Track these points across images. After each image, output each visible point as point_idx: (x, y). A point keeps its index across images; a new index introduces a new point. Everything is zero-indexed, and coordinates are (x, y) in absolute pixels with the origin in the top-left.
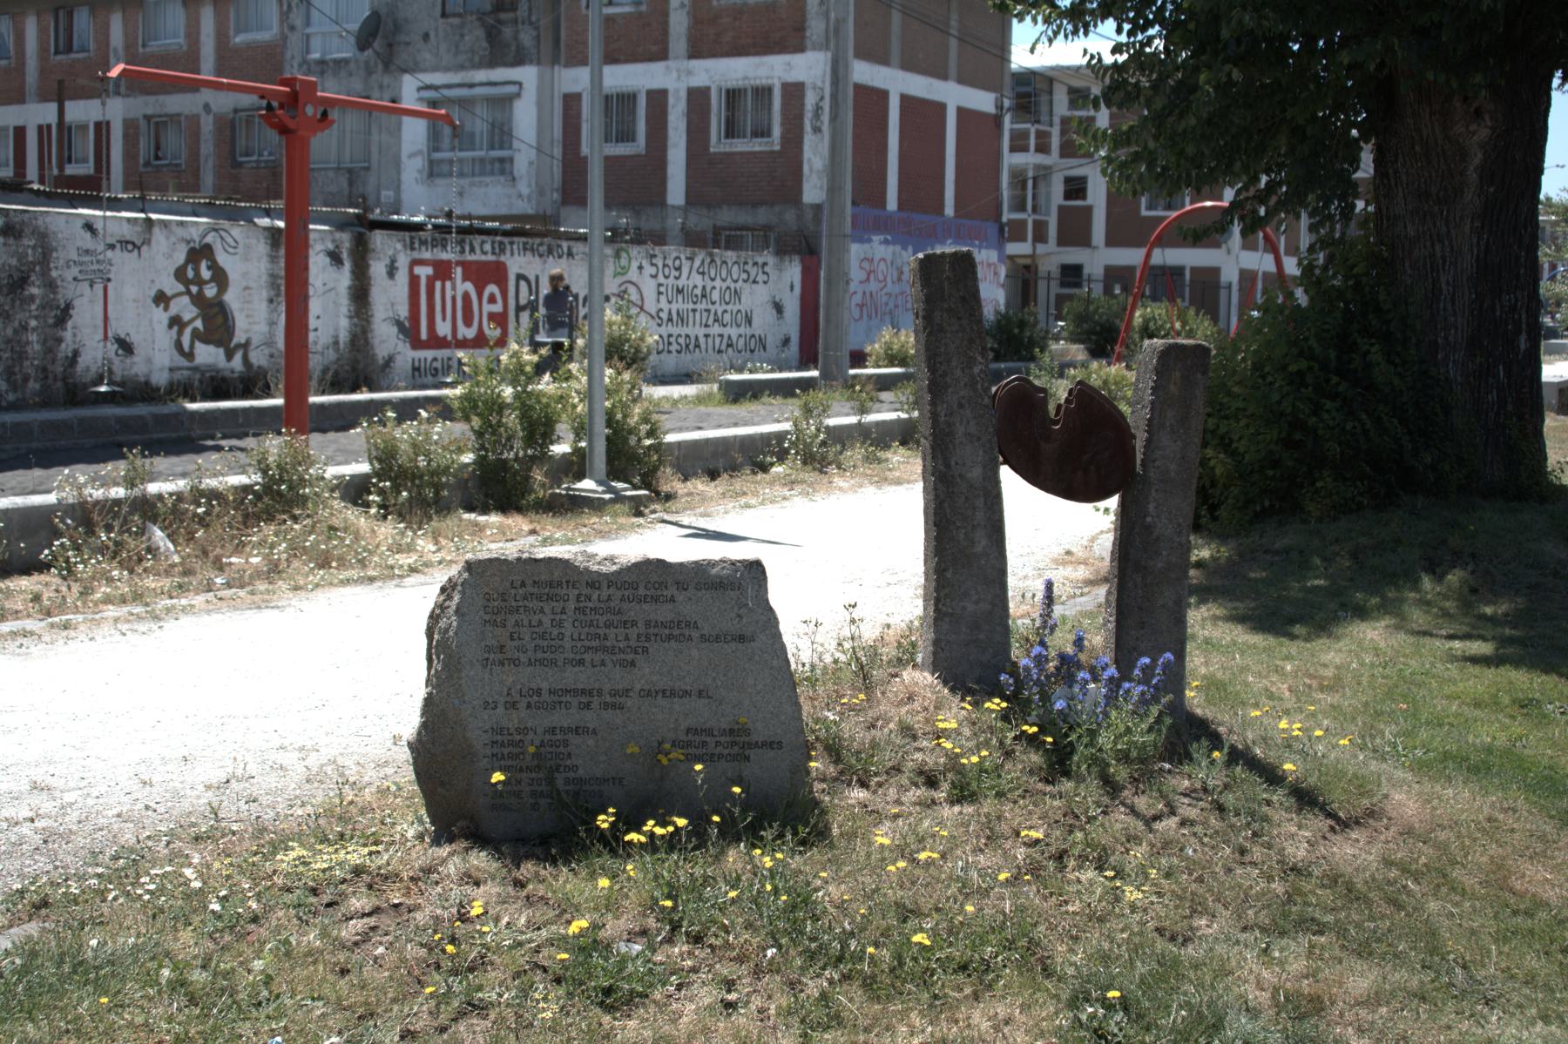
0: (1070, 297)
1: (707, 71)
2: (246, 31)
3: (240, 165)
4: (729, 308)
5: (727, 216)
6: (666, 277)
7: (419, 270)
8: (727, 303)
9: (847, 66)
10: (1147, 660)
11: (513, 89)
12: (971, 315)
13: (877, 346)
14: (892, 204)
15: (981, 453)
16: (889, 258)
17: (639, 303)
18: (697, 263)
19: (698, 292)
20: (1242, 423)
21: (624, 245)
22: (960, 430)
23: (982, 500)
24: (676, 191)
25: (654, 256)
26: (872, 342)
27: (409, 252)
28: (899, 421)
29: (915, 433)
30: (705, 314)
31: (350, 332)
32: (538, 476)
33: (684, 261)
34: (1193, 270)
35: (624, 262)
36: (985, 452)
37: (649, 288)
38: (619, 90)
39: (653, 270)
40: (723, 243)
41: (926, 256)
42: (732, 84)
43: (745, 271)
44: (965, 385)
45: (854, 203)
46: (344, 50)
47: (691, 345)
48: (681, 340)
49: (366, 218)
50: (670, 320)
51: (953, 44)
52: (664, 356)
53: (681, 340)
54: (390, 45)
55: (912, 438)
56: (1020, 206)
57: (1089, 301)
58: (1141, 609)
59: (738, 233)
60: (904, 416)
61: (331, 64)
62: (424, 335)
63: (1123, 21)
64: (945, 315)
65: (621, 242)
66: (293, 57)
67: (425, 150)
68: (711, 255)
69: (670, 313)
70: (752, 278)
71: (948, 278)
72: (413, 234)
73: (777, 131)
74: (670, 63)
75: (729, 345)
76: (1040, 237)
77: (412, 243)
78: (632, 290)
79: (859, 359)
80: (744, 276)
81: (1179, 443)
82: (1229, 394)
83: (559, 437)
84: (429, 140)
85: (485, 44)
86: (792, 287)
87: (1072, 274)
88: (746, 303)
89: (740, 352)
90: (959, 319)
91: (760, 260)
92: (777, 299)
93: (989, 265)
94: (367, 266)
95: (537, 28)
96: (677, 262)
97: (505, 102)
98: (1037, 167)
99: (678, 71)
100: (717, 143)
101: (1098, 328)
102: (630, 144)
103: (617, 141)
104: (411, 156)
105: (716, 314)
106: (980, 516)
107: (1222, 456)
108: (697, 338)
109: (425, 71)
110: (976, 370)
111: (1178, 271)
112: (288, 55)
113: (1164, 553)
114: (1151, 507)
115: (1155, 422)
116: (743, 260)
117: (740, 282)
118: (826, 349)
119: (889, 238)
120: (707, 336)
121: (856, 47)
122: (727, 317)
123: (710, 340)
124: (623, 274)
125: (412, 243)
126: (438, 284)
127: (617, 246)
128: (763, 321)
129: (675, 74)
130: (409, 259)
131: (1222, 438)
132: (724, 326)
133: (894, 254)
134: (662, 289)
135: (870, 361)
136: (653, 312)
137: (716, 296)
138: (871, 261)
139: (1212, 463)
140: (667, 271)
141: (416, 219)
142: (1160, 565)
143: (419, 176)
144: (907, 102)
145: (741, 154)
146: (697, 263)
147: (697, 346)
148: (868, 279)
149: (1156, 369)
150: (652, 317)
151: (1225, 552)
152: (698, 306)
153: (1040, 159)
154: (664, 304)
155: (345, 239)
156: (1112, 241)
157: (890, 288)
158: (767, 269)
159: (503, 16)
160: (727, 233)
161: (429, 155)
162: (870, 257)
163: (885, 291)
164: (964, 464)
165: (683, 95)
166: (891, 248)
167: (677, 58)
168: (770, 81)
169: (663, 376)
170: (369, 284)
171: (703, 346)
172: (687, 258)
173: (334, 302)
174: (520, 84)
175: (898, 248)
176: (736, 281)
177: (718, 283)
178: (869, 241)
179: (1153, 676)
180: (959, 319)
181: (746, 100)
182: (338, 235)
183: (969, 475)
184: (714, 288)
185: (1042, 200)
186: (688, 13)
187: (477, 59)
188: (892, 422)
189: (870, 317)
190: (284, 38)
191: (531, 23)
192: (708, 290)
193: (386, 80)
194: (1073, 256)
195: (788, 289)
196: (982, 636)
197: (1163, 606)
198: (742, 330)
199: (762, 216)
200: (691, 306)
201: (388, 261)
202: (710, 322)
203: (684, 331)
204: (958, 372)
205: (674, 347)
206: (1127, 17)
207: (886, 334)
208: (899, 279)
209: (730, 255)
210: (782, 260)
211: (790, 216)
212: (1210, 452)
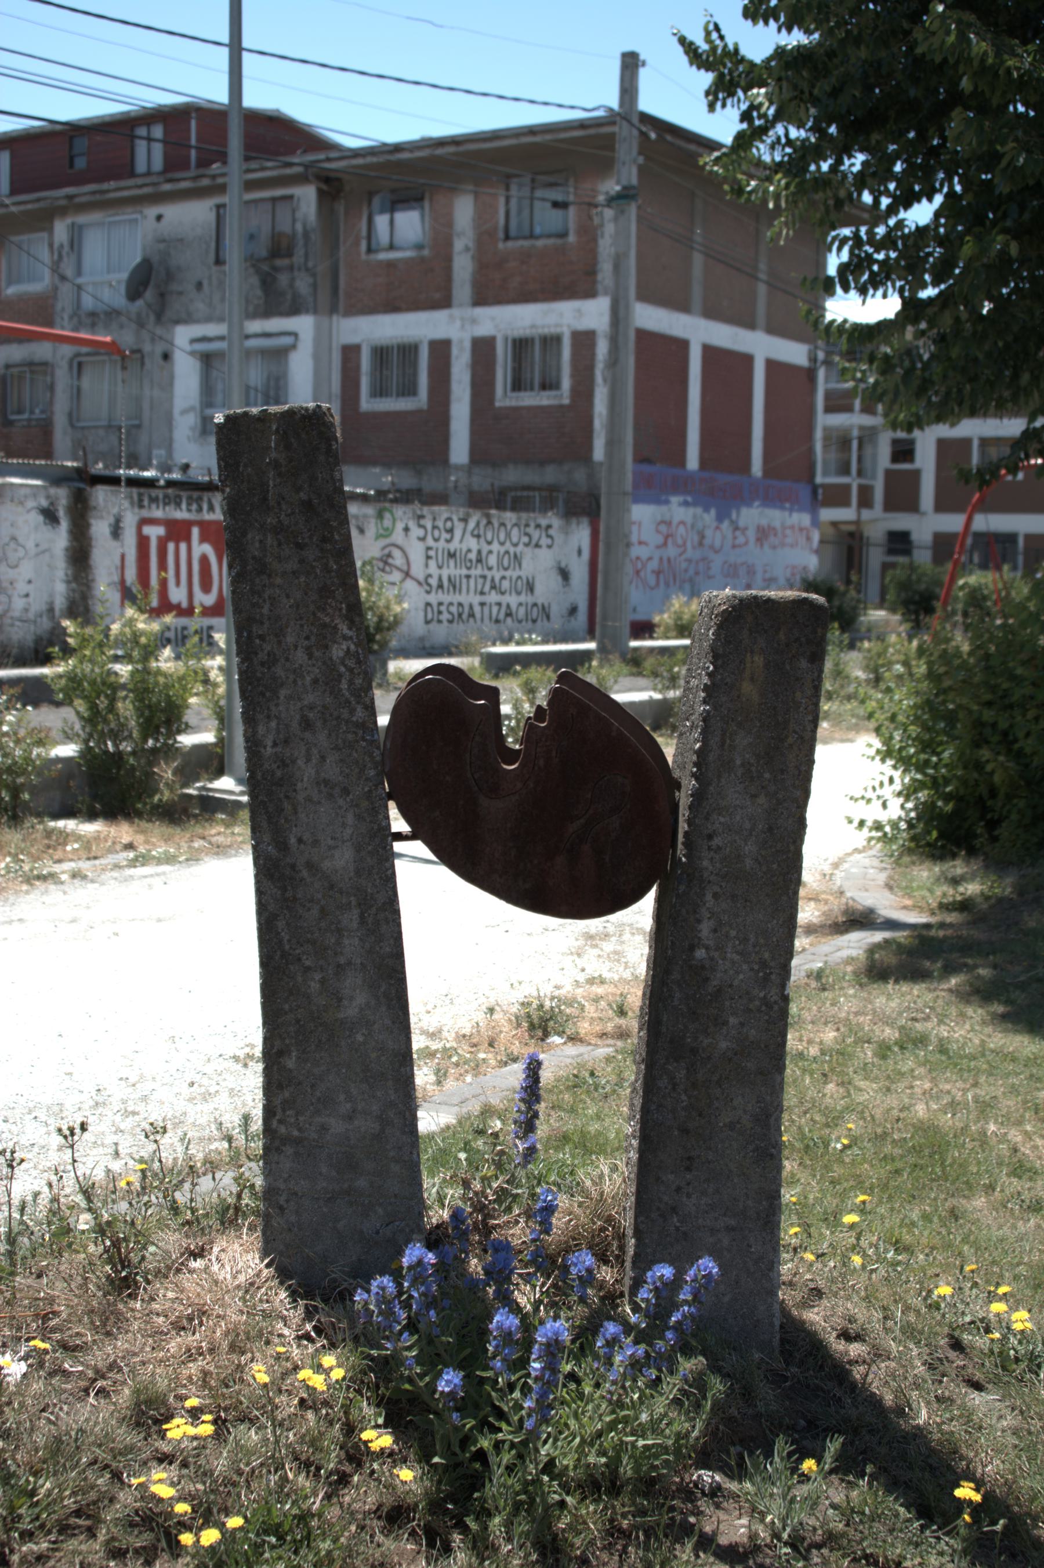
0: (893, 566)
1: (493, 319)
2: (19, 281)
3: (11, 423)
4: (508, 574)
5: (513, 475)
6: (436, 540)
7: (148, 530)
8: (506, 569)
9: (627, 307)
10: (666, 1271)
11: (287, 340)
12: (324, 540)
13: (666, 616)
14: (693, 461)
15: (350, 819)
16: (689, 520)
17: (405, 568)
18: (472, 525)
19: (473, 556)
20: (1031, 714)
21: (387, 505)
22: (306, 772)
23: (355, 913)
24: (460, 450)
25: (421, 517)
26: (662, 612)
27: (136, 510)
28: (651, 702)
29: (670, 716)
30: (480, 581)
31: (68, 598)
32: (166, 772)
33: (456, 522)
34: (1028, 537)
35: (387, 522)
36: (359, 817)
37: (416, 552)
38: (399, 340)
39: (421, 532)
40: (509, 504)
41: (228, 418)
42: (519, 333)
43: (527, 534)
44: (315, 681)
45: (641, 459)
46: (117, 298)
47: (464, 615)
48: (454, 609)
49: (87, 472)
50: (440, 586)
51: (762, 289)
52: (433, 626)
53: (454, 609)
54: (162, 295)
55: (666, 722)
56: (844, 469)
57: (912, 567)
58: (685, 1131)
59: (525, 493)
60: (657, 696)
61: (102, 316)
62: (155, 602)
63: (881, 194)
64: (270, 540)
65: (385, 500)
66: (63, 309)
67: (198, 405)
68: (488, 516)
69: (440, 579)
70: (534, 542)
71: (276, 464)
72: (142, 490)
73: (566, 383)
74: (455, 311)
75: (509, 614)
76: (865, 500)
77: (141, 501)
78: (397, 553)
79: (643, 629)
80: (526, 539)
81: (762, 800)
82: (1012, 677)
83: (187, 726)
84: (201, 394)
85: (259, 292)
86: (580, 552)
87: (899, 542)
88: (528, 568)
89: (520, 622)
90: (300, 546)
91: (544, 522)
92: (563, 565)
93: (801, 529)
94: (88, 526)
95: (314, 275)
96: (449, 524)
97: (279, 355)
98: (862, 428)
99: (462, 319)
100: (503, 397)
101: (917, 598)
102: (411, 399)
103: (398, 395)
104: (184, 412)
105: (493, 580)
106: (352, 946)
107: (1001, 758)
108: (471, 607)
109: (197, 321)
110: (337, 652)
111: (1010, 538)
112: (59, 306)
113: (733, 1020)
114: (705, 929)
115: (711, 757)
116: (523, 522)
117: (521, 547)
118: (605, 618)
119: (689, 499)
120: (482, 604)
121: (639, 286)
122: (506, 584)
123: (486, 609)
124: (386, 536)
125: (141, 501)
126: (171, 547)
127: (379, 505)
128: (547, 589)
129: (458, 323)
130: (136, 519)
131: (1005, 734)
132: (503, 593)
133: (695, 516)
134: (432, 553)
135: (659, 631)
136: (421, 578)
137: (493, 560)
138: (669, 524)
139: (989, 768)
140: (436, 533)
141: (147, 474)
142: (723, 1045)
143: (190, 434)
144: (711, 353)
145: (530, 409)
146: (472, 525)
147: (472, 615)
148: (665, 544)
149: (713, 649)
150: (420, 583)
151: (1005, 887)
152: (473, 572)
153: (867, 420)
154: (433, 568)
155: (62, 495)
156: (942, 506)
157: (690, 553)
158: (551, 532)
159: (279, 262)
160: (513, 494)
161: (202, 411)
162: (667, 518)
163: (684, 557)
164: (316, 843)
165: (467, 345)
166: (691, 511)
167: (461, 305)
168: (558, 330)
169: (433, 648)
170: (90, 545)
171: (478, 615)
172: (460, 520)
173: (49, 566)
174: (295, 335)
175: (699, 510)
176: (516, 545)
177: (495, 547)
178: (667, 502)
179: (676, 1306)
180: (300, 546)
181: (533, 351)
182: (53, 491)
183: (326, 865)
184: (490, 552)
185: (868, 463)
186: (473, 257)
187: (251, 309)
188: (642, 704)
189: (667, 584)
190: (56, 289)
191: (307, 270)
192: (484, 554)
193: (159, 331)
194: (901, 522)
195: (575, 554)
196: (362, 1183)
197: (731, 1126)
198: (523, 598)
199: (550, 475)
200: (464, 572)
201: (112, 520)
202: (487, 588)
203: (457, 598)
204: (300, 657)
205: (445, 616)
206: (887, 190)
207: (677, 602)
208: (701, 544)
209: (510, 517)
210: (568, 523)
211: (580, 475)
212: (985, 754)
